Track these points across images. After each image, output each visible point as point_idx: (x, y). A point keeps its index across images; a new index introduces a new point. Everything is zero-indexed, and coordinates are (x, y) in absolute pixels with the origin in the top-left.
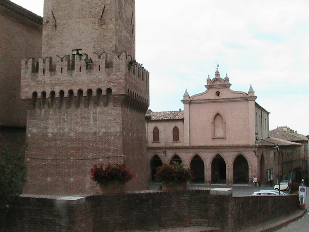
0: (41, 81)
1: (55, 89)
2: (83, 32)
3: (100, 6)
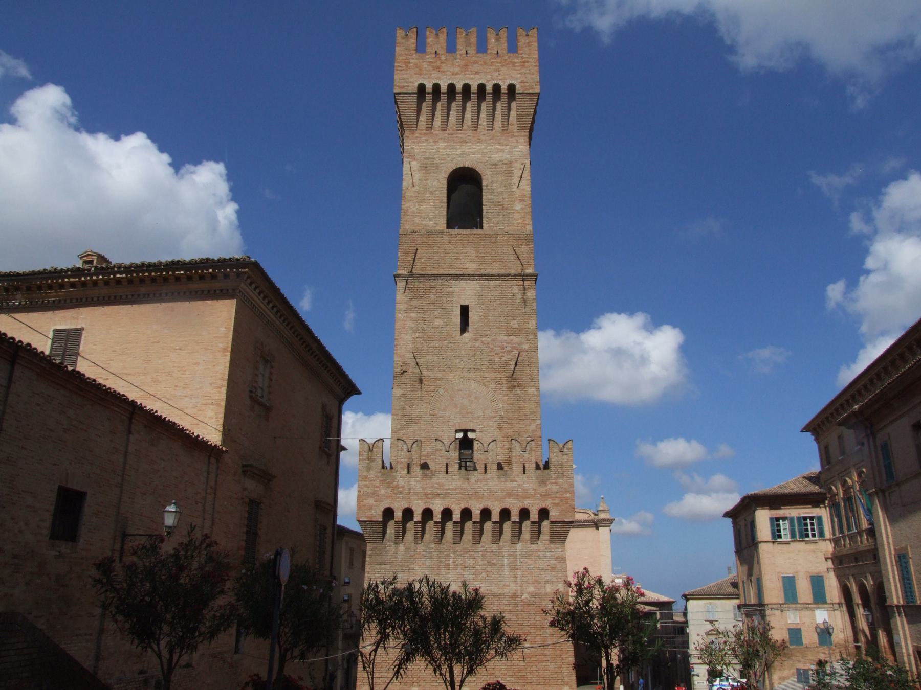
0: (403, 487)
1: (433, 504)
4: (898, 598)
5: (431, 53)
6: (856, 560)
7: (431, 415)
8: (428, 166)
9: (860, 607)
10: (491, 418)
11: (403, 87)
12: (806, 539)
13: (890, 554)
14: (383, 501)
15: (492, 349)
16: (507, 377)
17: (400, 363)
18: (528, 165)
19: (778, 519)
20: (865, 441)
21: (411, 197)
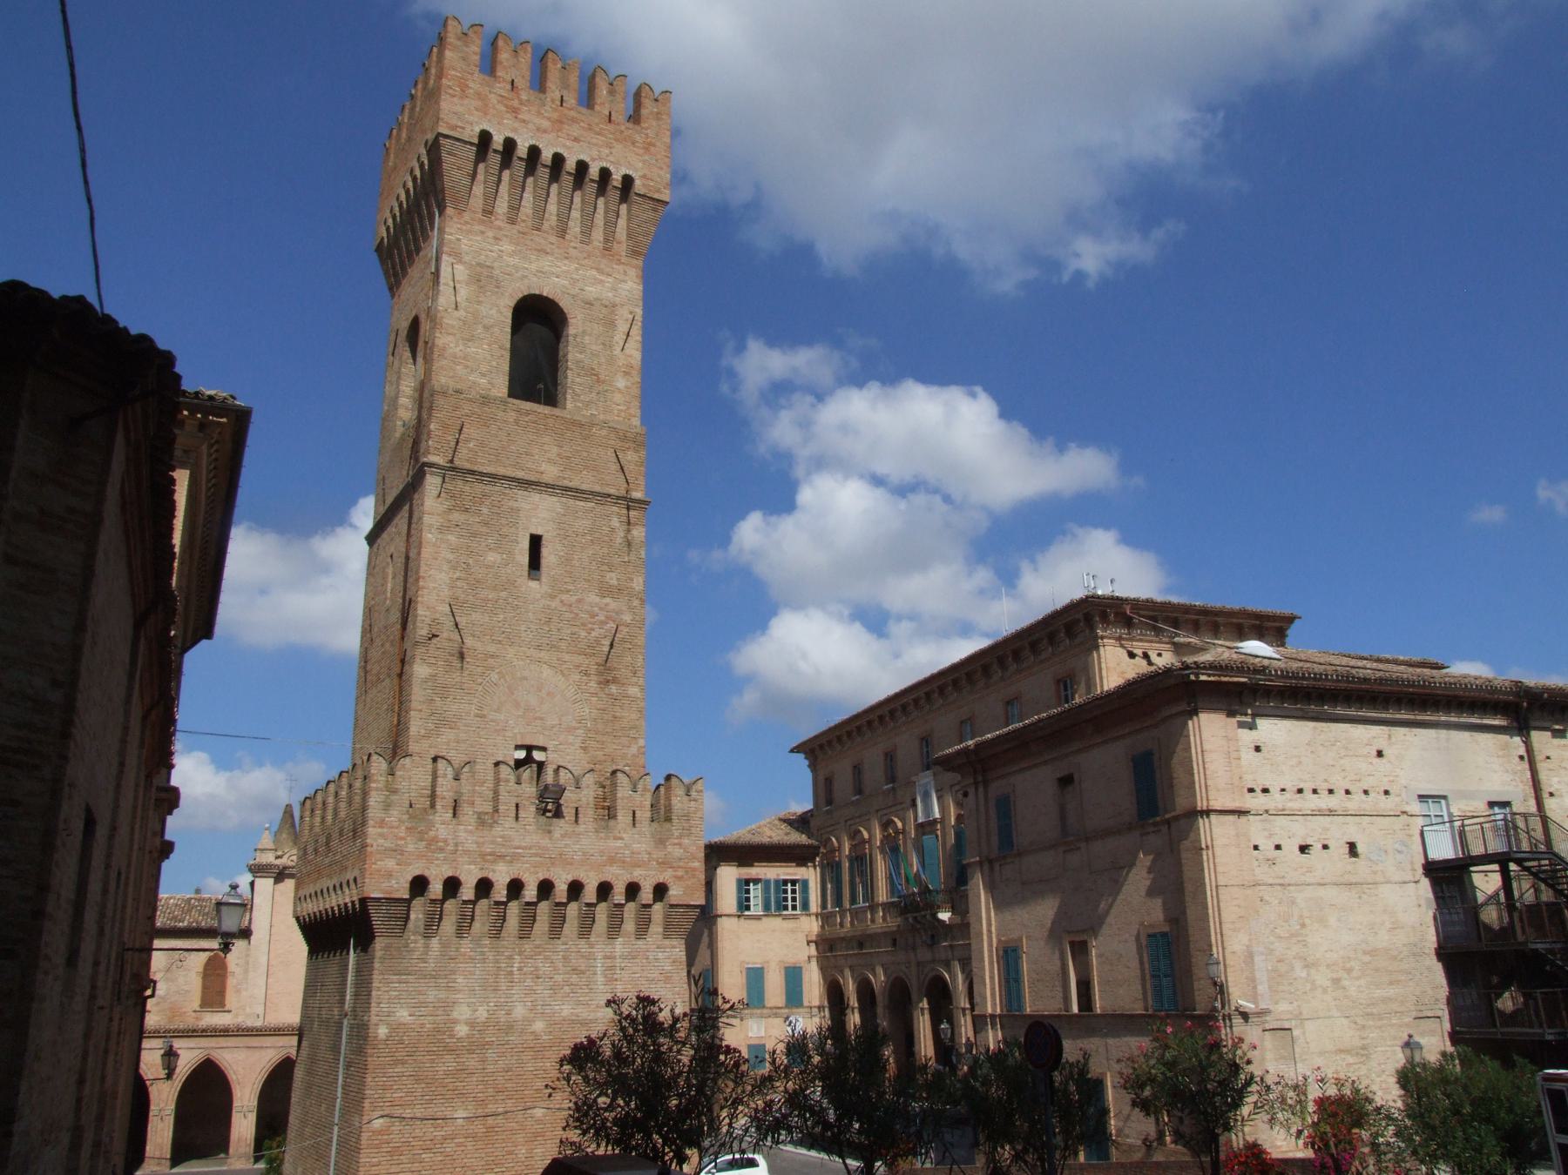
0: (445, 841)
1: (494, 871)
3: (604, 623)
4: (994, 1005)
5: (504, 80)
6: (861, 945)
7: (477, 716)
8: (483, 278)
9: (856, 1011)
10: (570, 730)
11: (454, 128)
12: (785, 913)
13: (990, 945)
14: (410, 864)
15: (577, 615)
16: (597, 664)
17: (428, 620)
18: (639, 318)
19: (747, 882)
20: (971, 791)
21: (453, 327)
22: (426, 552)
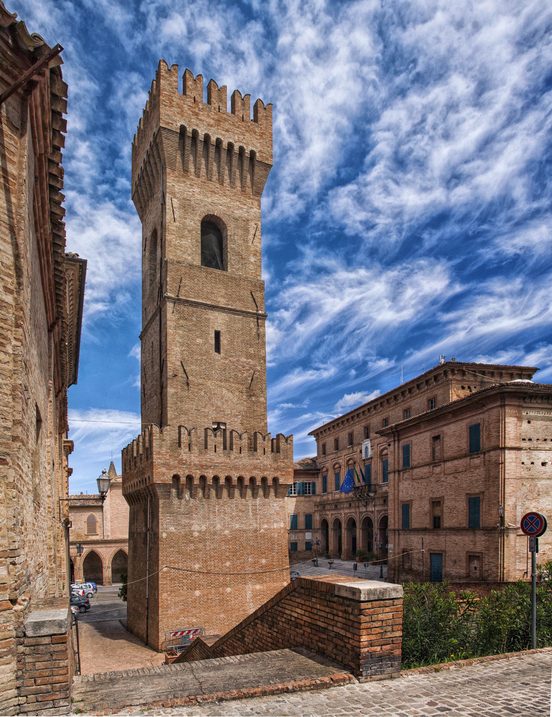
0: (186, 460)
2: (226, 401)
5: (191, 97)
11: (168, 123)
20: (392, 444)
21: (174, 230)
22: (169, 338)
